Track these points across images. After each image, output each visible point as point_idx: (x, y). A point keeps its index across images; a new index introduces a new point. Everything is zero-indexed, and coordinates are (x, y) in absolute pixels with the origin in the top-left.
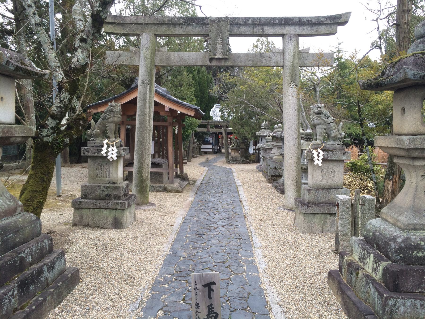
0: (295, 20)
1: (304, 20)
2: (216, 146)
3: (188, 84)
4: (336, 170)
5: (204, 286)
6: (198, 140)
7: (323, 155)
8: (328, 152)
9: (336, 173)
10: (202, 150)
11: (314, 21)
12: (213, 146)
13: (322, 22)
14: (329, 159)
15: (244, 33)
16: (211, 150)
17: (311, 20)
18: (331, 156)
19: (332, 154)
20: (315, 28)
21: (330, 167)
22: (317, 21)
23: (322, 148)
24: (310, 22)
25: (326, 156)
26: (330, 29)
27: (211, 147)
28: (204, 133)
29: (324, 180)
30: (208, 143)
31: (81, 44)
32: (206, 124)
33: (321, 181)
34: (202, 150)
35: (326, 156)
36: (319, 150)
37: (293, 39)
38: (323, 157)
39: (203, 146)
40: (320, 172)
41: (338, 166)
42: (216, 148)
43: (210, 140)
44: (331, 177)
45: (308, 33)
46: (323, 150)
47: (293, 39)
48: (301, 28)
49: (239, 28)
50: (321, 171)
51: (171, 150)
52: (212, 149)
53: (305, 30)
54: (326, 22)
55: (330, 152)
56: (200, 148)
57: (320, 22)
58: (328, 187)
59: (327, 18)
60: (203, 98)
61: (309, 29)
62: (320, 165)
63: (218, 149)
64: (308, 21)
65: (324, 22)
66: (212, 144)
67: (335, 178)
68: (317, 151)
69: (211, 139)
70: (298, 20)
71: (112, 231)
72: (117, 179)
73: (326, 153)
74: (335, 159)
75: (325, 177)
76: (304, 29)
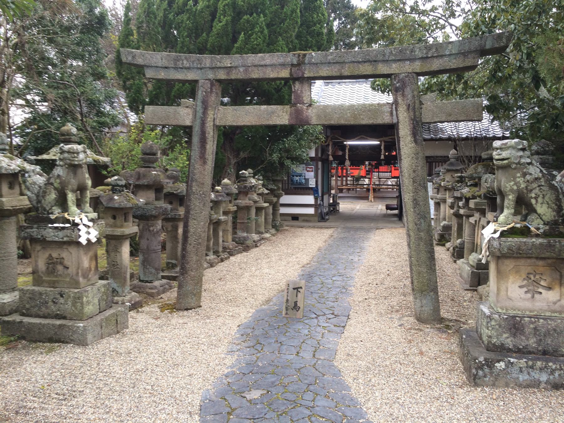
2: (326, 197)
3: (259, 347)
5: (294, 289)
6: (266, 178)
10: (283, 210)
12: (316, 199)
16: (311, 211)
27: (310, 199)
28: (276, 133)
30: (301, 189)
32: (285, 73)
34: (283, 210)
39: (286, 199)
42: (326, 203)
43: (307, 180)
52: (316, 206)
56: (275, 206)
60: (283, 21)
63: (330, 205)
66: (314, 191)
69: (310, 175)
71: (123, 254)
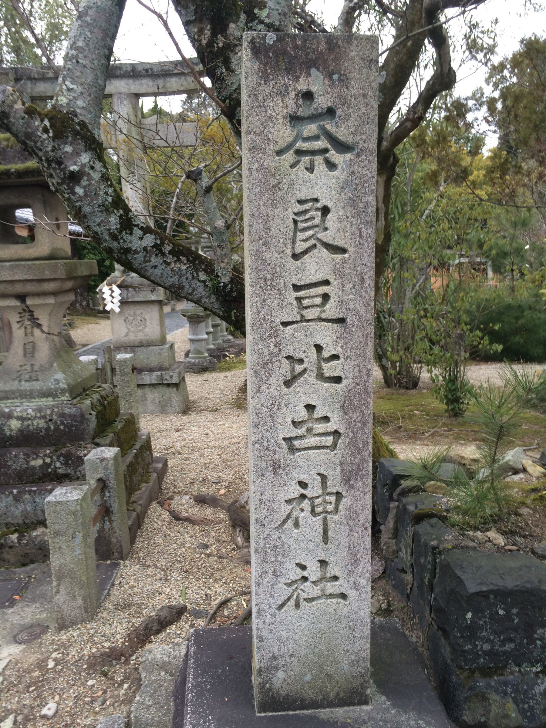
0: (124, 69)
1: (140, 68)
4: (147, 316)
7: (120, 295)
8: (127, 290)
9: (148, 322)
11: (155, 69)
13: (169, 70)
14: (130, 300)
15: (45, 93)
17: (151, 69)
18: (133, 296)
19: (134, 293)
20: (160, 82)
21: (138, 312)
22: (162, 70)
23: (118, 283)
24: (150, 72)
25: (125, 296)
26: (185, 83)
29: (131, 334)
31: (377, 33)
33: (127, 335)
35: (125, 296)
36: (114, 287)
37: (125, 102)
38: (120, 298)
40: (123, 321)
41: (149, 310)
44: (141, 328)
45: (150, 90)
46: (119, 287)
47: (125, 102)
48: (137, 82)
49: (35, 85)
50: (125, 321)
51: (9, 301)
53: (145, 86)
54: (176, 71)
55: (130, 289)
57: (166, 71)
58: (138, 344)
59: (176, 65)
61: (151, 83)
62: (117, 310)
64: (147, 71)
65: (173, 71)
67: (147, 330)
68: (111, 289)
70: (129, 69)
72: (419, 379)
73: (125, 291)
74: (139, 299)
75: (132, 329)
76: (142, 84)
